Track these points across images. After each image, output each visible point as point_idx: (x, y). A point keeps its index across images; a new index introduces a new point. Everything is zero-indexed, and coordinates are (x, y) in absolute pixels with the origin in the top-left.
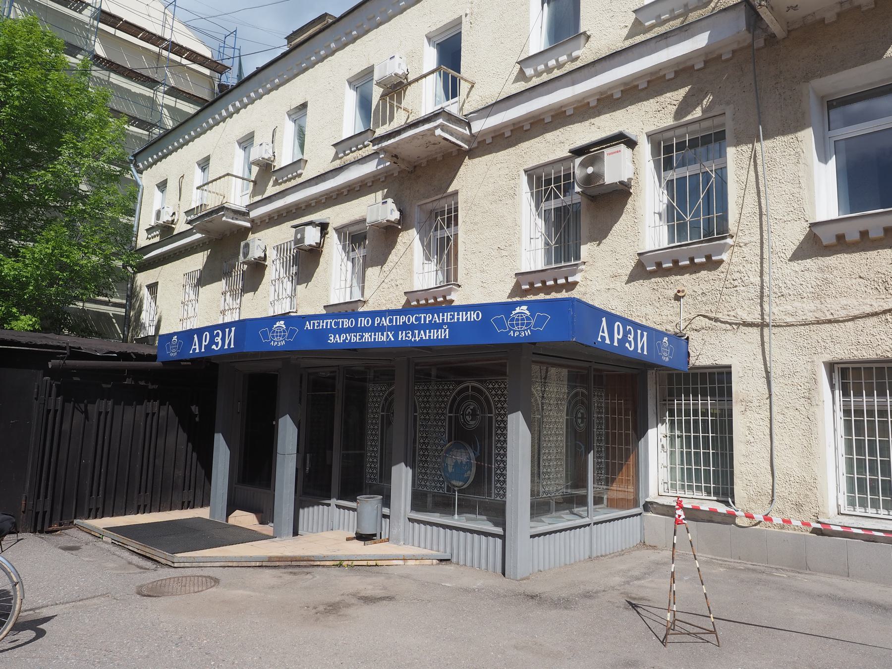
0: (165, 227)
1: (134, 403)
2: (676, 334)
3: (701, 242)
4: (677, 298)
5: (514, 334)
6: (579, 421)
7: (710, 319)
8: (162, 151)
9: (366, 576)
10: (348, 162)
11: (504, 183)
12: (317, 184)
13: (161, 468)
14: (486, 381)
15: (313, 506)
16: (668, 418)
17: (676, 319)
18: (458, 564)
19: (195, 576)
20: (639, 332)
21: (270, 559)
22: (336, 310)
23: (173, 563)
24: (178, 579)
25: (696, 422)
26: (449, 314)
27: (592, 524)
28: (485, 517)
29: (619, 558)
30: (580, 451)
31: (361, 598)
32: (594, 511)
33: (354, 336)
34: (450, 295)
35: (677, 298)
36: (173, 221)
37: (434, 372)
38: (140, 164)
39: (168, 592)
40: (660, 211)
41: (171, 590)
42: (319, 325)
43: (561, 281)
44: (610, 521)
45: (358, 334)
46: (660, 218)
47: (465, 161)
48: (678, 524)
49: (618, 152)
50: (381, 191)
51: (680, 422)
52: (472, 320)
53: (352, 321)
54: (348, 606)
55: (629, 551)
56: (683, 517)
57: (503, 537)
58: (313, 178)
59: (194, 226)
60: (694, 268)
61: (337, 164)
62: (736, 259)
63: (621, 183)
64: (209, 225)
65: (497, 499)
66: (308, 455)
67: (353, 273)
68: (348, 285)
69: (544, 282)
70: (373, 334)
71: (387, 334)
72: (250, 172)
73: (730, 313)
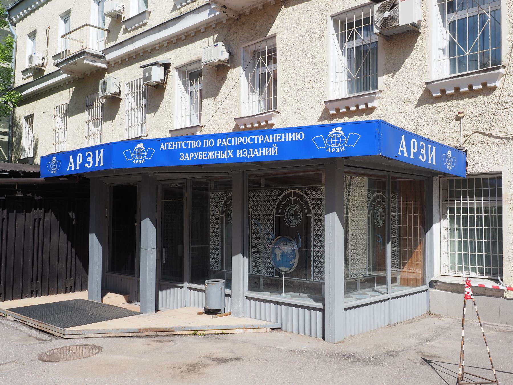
0: (37, 69)
1: (50, 210)
2: (457, 147)
3: (479, 72)
4: (458, 119)
5: (331, 150)
7: (485, 135)
8: (31, 6)
9: (216, 342)
10: (185, 12)
11: (314, 27)
12: (159, 31)
14: (305, 188)
15: (169, 288)
16: (449, 215)
17: (457, 136)
19: (82, 345)
20: (430, 146)
21: (140, 331)
22: (179, 134)
23: (65, 335)
24: (70, 348)
25: (472, 218)
27: (391, 299)
28: (306, 295)
29: (411, 325)
30: (379, 242)
31: (214, 360)
32: (392, 289)
34: (271, 120)
35: (458, 119)
36: (43, 64)
37: (263, 182)
38: (14, 18)
39: (63, 358)
40: (444, 47)
41: (65, 357)
42: (172, 146)
43: (362, 107)
44: (404, 296)
45: (204, 153)
46: (444, 53)
47: (282, 9)
48: (467, 299)
51: (459, 218)
52: (297, 139)
53: (198, 142)
54: (205, 366)
55: (419, 318)
56: (471, 293)
57: (323, 311)
58: (157, 26)
59: (61, 68)
60: (472, 93)
61: (176, 14)
62: (508, 86)
63: (413, 24)
64: (73, 67)
66: (164, 249)
67: (191, 104)
68: (188, 114)
69: (348, 108)
70: (216, 152)
71: (228, 152)
72: (104, 22)
73: (501, 130)
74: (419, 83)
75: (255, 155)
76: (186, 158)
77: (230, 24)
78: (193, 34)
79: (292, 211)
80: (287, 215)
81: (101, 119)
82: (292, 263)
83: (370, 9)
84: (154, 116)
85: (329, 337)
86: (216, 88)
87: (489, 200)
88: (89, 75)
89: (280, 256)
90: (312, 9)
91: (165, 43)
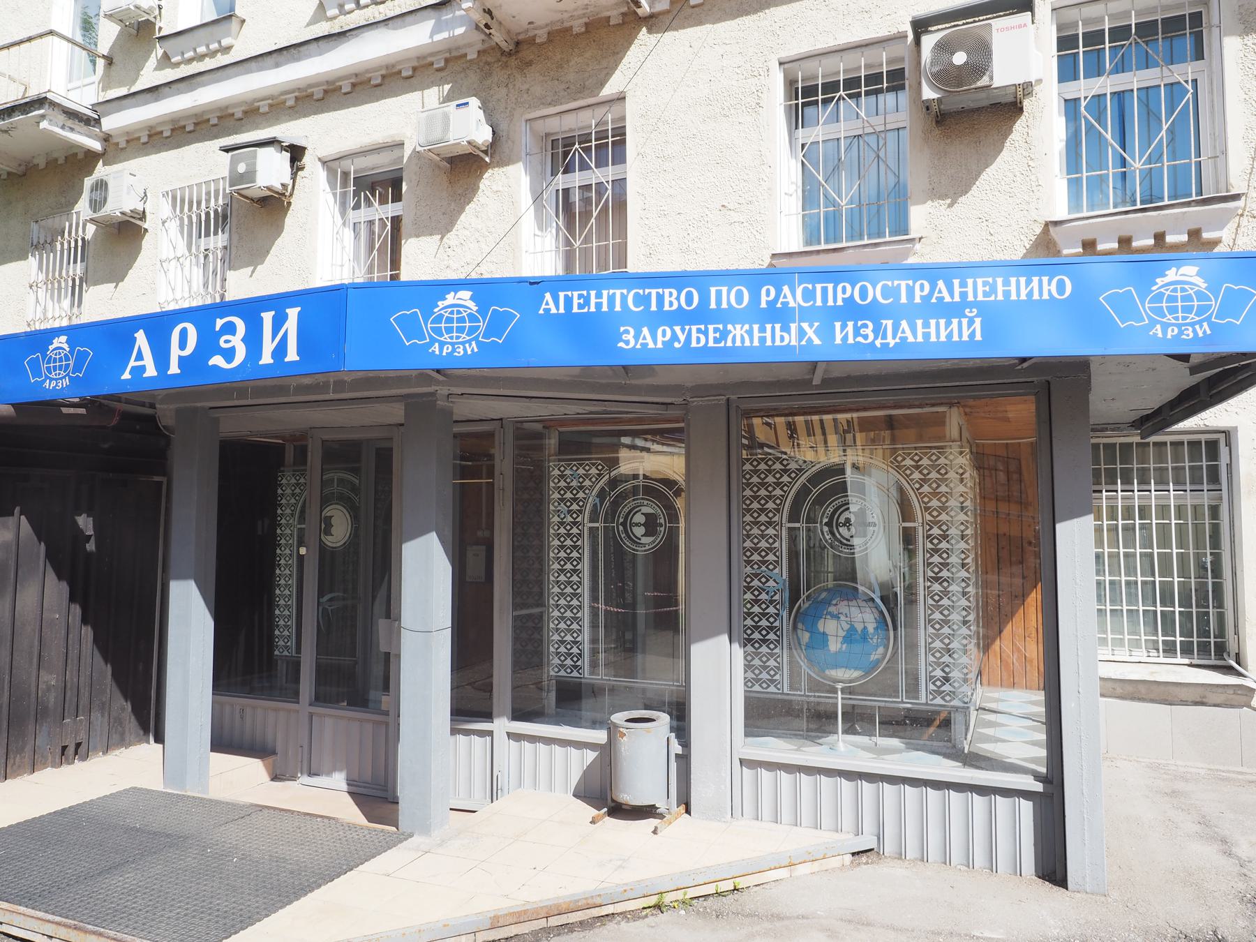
1: (17, 510)
6: (639, 531)
12: (277, 65)
13: (7, 671)
18: (900, 856)
26: (980, 281)
33: (699, 331)
45: (711, 327)
49: (1020, 26)
50: (436, 89)
52: (1046, 296)
61: (323, 28)
65: (935, 702)
70: (756, 327)
74: (1022, 225)
75: (900, 338)
76: (641, 341)
77: (488, 64)
78: (376, 79)
79: (640, 513)
80: (624, 524)
81: (81, 279)
82: (876, 657)
83: (884, 53)
84: (251, 276)
85: (1084, 878)
86: (444, 214)
87: (1188, 491)
88: (42, 166)
89: (840, 639)
90: (727, 42)
91: (289, 99)
